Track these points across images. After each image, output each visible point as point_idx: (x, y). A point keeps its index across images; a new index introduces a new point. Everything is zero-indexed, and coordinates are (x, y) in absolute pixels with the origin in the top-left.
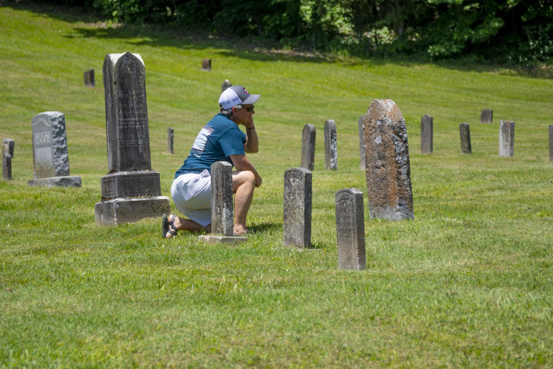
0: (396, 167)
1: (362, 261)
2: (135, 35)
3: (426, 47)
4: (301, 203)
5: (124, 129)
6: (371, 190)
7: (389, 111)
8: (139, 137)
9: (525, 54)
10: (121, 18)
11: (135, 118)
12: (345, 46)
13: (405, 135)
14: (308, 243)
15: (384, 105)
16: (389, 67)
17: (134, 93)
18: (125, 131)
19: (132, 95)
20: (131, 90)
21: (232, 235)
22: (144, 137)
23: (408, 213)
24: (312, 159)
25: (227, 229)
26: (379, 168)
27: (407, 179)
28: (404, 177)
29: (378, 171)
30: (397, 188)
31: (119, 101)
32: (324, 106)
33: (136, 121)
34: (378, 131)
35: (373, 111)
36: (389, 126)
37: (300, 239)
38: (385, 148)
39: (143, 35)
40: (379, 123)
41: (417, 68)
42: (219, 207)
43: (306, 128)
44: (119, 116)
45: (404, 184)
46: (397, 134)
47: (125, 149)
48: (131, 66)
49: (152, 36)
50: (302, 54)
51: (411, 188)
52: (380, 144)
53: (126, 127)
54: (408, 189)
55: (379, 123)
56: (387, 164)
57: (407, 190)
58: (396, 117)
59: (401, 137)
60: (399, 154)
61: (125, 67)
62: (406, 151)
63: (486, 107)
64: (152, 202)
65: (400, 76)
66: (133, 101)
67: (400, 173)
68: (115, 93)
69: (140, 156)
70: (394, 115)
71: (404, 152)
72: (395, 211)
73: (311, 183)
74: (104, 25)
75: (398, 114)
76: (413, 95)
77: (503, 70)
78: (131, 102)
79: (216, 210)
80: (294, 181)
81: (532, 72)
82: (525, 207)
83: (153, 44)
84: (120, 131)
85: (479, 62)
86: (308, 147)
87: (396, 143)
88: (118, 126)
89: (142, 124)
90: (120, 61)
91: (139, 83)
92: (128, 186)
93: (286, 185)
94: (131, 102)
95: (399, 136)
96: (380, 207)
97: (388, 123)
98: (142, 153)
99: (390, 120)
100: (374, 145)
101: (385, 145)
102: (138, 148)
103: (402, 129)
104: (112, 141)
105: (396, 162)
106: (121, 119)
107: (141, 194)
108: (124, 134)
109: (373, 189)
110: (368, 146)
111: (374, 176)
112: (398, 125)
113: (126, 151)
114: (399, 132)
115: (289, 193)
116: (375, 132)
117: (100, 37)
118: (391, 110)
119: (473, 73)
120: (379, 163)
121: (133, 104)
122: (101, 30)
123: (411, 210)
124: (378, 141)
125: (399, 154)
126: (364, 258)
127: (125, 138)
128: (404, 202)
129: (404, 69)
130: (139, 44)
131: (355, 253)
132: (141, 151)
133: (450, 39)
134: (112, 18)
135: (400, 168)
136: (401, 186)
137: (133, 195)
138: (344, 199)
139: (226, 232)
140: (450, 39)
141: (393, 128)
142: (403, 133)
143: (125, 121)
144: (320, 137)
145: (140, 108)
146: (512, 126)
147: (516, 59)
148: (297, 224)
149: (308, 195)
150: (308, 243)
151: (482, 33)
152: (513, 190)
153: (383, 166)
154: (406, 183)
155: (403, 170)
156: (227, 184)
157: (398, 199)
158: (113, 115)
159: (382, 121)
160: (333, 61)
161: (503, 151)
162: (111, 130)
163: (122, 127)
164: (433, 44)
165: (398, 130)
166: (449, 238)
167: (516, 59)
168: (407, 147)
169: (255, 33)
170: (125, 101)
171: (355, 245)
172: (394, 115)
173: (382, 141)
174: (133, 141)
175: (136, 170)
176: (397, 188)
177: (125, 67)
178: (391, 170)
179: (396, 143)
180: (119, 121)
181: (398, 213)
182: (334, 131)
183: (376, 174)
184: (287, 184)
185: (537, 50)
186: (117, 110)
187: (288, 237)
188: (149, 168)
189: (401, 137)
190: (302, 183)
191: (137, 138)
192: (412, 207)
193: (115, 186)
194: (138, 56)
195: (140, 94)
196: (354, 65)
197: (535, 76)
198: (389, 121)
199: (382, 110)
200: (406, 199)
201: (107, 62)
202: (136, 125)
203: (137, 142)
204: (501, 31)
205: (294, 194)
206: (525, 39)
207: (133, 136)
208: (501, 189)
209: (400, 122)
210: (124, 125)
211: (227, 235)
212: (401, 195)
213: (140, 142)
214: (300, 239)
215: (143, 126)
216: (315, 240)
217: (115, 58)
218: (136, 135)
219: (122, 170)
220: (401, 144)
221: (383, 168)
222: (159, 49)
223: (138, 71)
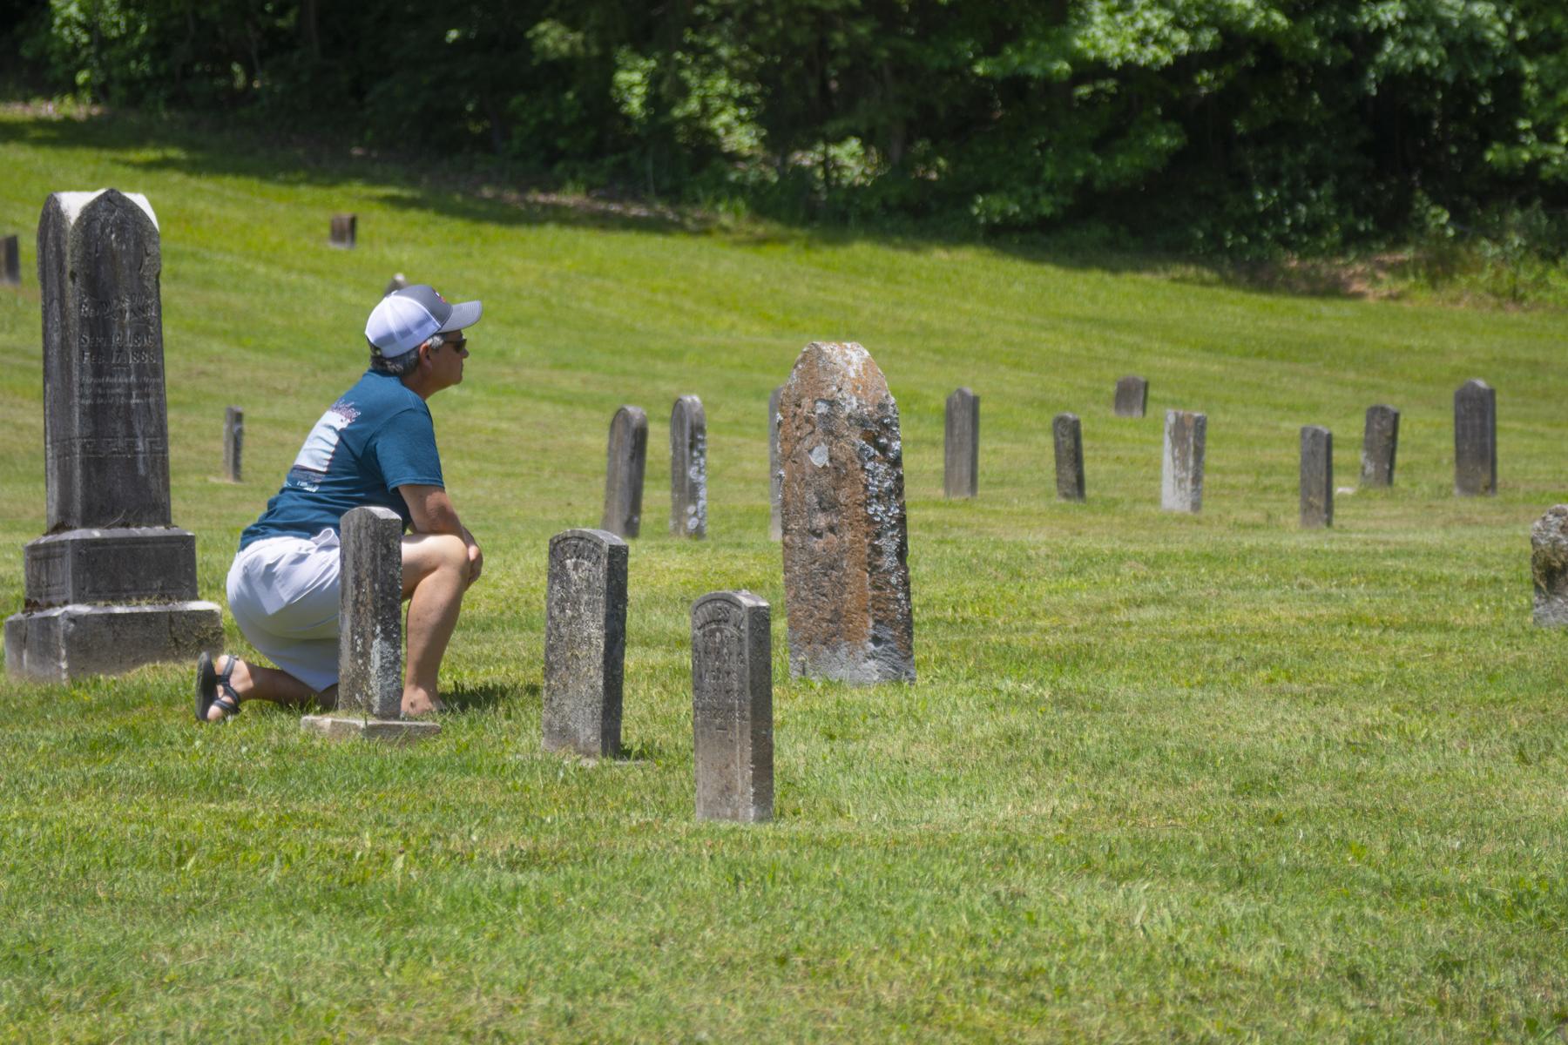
1: (763, 797)
2: (139, 141)
3: (965, 199)
4: (594, 630)
5: (94, 407)
6: (796, 596)
7: (853, 375)
8: (138, 432)
9: (1241, 226)
10: (101, 92)
11: (129, 376)
12: (738, 189)
13: (896, 445)
14: (613, 745)
15: (839, 360)
16: (862, 251)
17: (126, 305)
18: (98, 413)
19: (122, 312)
20: (118, 298)
21: (397, 717)
23: (900, 663)
24: (635, 505)
25: (382, 700)
26: (820, 536)
28: (888, 562)
29: (818, 545)
31: (82, 326)
32: (674, 355)
33: (129, 387)
34: (819, 430)
35: (807, 375)
36: (850, 417)
37: (588, 732)
38: (839, 479)
39: (162, 141)
41: (939, 257)
42: (362, 635)
43: (621, 416)
44: (82, 370)
45: (888, 583)
46: (873, 440)
47: (96, 464)
48: (121, 228)
49: (189, 145)
50: (615, 208)
51: (908, 593)
52: (824, 467)
53: (100, 401)
54: (900, 595)
55: (822, 408)
57: (898, 600)
58: (871, 394)
59: (884, 449)
60: (878, 497)
62: (898, 490)
63: (1129, 372)
64: (172, 617)
65: (891, 277)
66: (122, 327)
67: (878, 551)
70: (865, 387)
71: (891, 491)
72: (861, 658)
74: (49, 109)
76: (926, 332)
77: (1179, 270)
80: (576, 567)
81: (1256, 274)
82: (1225, 654)
83: (193, 168)
84: (83, 413)
85: (1113, 245)
86: (623, 471)
89: (148, 395)
90: (90, 212)
91: (141, 278)
92: (103, 571)
94: (116, 329)
95: (877, 446)
96: (819, 647)
97: (848, 410)
98: (146, 479)
100: (808, 471)
101: (837, 470)
103: (887, 427)
104: (60, 442)
106: (88, 380)
107: (141, 593)
108: (96, 423)
109: (803, 594)
111: (805, 557)
112: (876, 416)
114: (880, 436)
115: (562, 600)
117: (38, 143)
118: (857, 372)
119: (1095, 276)
120: (821, 521)
121: (123, 337)
122: (41, 123)
123: (908, 657)
124: (819, 458)
125: (878, 497)
128: (887, 633)
129: (906, 259)
130: (149, 166)
131: (743, 774)
132: (142, 471)
133: (1034, 178)
134: (74, 89)
135: (878, 536)
136: (880, 588)
137: (116, 599)
138: (718, 620)
139: (381, 707)
140: (1034, 178)
141: (862, 422)
144: (659, 443)
146: (1200, 426)
147: (1215, 238)
148: (583, 688)
150: (613, 745)
151: (1124, 164)
152: (1196, 607)
153: (831, 529)
154: (893, 580)
155: (889, 544)
157: (871, 623)
158: (66, 367)
159: (832, 403)
160: (704, 229)
161: (1173, 496)
162: (57, 408)
163: (88, 402)
164: (985, 189)
165: (875, 428)
166: (1011, 738)
167: (1215, 238)
168: (900, 479)
169: (484, 143)
170: (99, 327)
171: (743, 755)
172: (865, 387)
173: (831, 459)
175: (127, 525)
178: (852, 542)
179: (869, 466)
180: (82, 385)
181: (872, 663)
182: (698, 429)
183: (812, 552)
184: (557, 574)
185: (1274, 214)
186: (75, 353)
188: (166, 521)
189: (884, 449)
190: (601, 572)
191: (131, 434)
192: (910, 648)
193: (65, 571)
194: (140, 200)
195: (143, 309)
196: (761, 241)
197: (1267, 287)
198: (851, 404)
199: (832, 372)
200: (893, 623)
201: (51, 215)
202: (129, 396)
203: (132, 446)
204: (1176, 158)
205: (576, 603)
206: (1242, 183)
207: (120, 427)
208: (1161, 601)
210: (95, 396)
211: (382, 716)
213: (141, 446)
214: (589, 731)
215: (152, 400)
216: (631, 735)
217: (74, 203)
218: (129, 425)
219: (87, 523)
220: (882, 468)
221: (831, 535)
222: (207, 184)
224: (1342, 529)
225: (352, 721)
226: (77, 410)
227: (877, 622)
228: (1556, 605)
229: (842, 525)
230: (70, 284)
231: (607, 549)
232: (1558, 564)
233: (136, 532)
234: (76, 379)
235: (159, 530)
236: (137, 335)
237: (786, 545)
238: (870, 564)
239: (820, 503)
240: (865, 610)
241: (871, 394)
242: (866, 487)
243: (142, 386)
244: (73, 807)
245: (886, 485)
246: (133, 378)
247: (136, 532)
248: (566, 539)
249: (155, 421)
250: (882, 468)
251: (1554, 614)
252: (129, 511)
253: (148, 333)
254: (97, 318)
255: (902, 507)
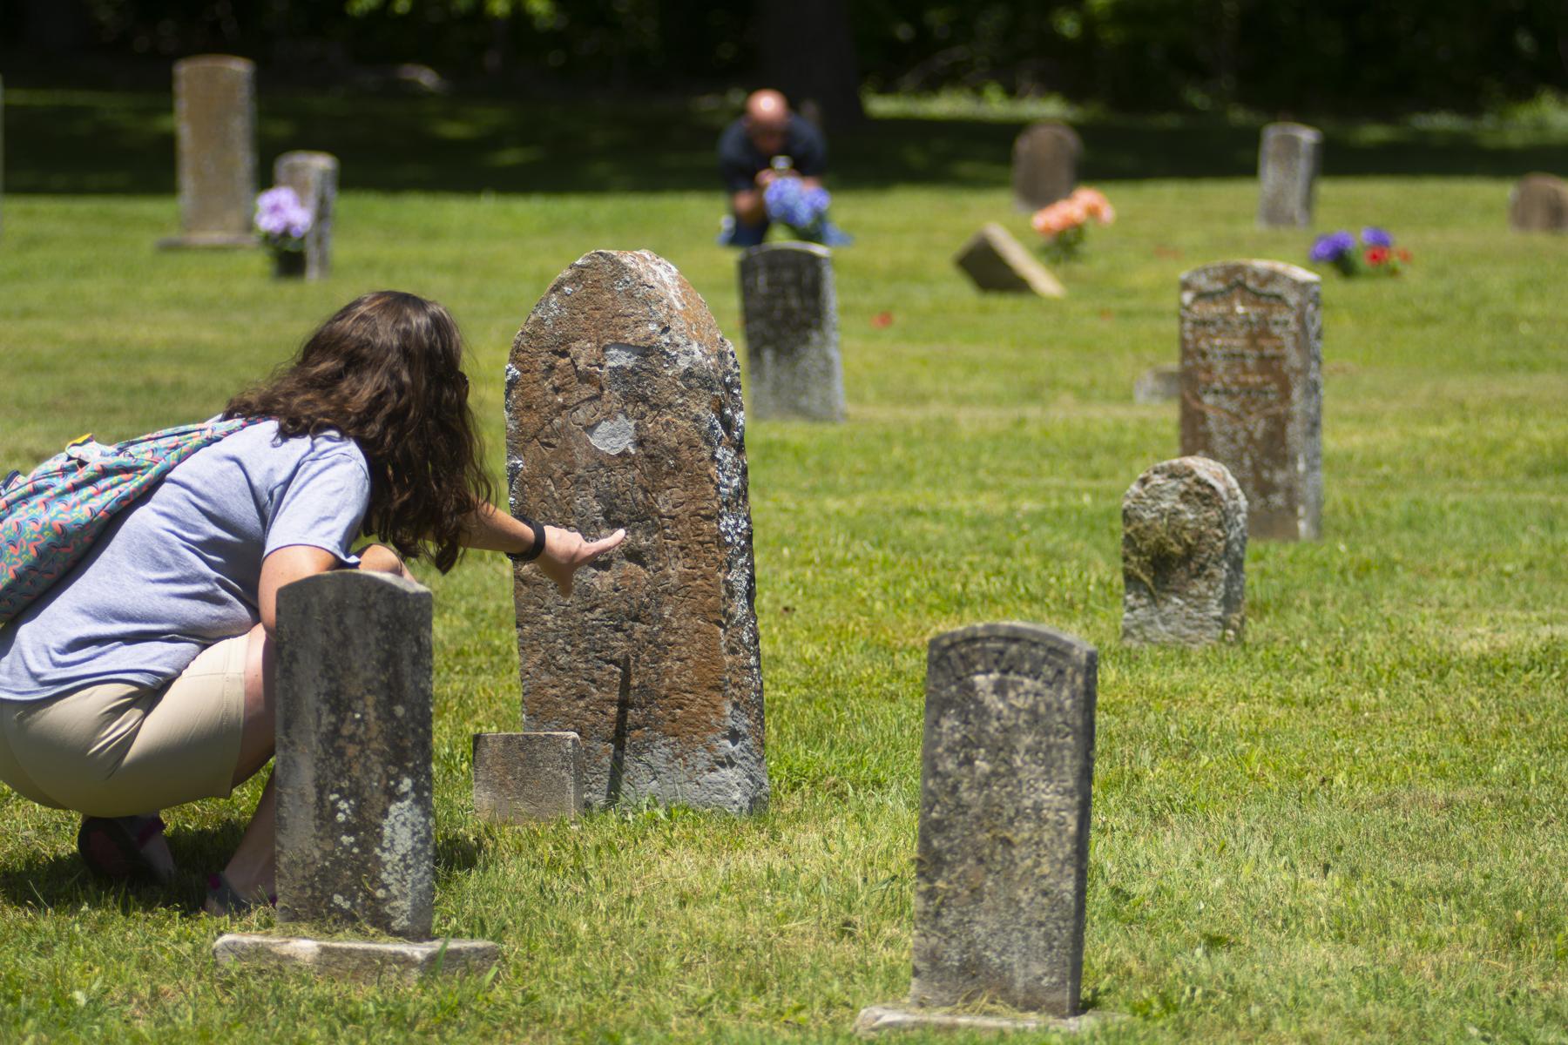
6: (546, 665)
36: (688, 374)
37: (1033, 968)
38: (656, 474)
42: (354, 793)
52: (624, 454)
55: (621, 359)
79: (325, 814)
80: (1000, 689)
93: (937, 706)
97: (683, 363)
100: (582, 459)
109: (562, 659)
115: (966, 743)
156: (416, 684)
173: (640, 443)
178: (685, 577)
187: (953, 957)
199: (646, 302)
205: (1002, 749)
214: (1038, 969)
216: (1096, 978)
221: (631, 567)
224: (1090, 524)
225: (277, 942)
228: (1169, 609)
232: (1177, 549)
239: (606, 514)
248: (972, 640)
251: (1165, 622)
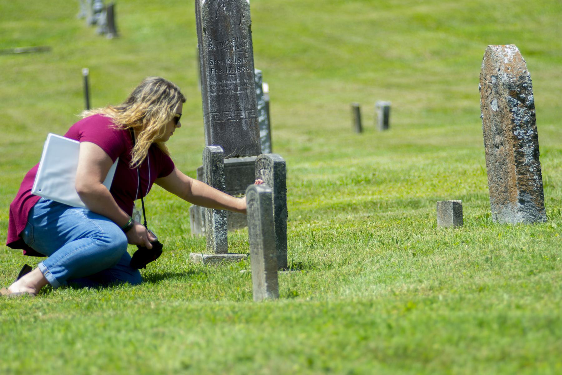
0: (514, 146)
5: (218, 96)
6: (491, 180)
7: (506, 61)
8: (242, 108)
11: (236, 80)
13: (530, 98)
15: (500, 54)
17: (233, 43)
19: (231, 47)
20: (228, 40)
21: (226, 252)
22: (249, 107)
23: (536, 213)
25: (217, 244)
27: (533, 163)
28: (527, 160)
29: (497, 152)
30: (517, 177)
31: (210, 56)
33: (236, 85)
34: (493, 92)
40: (494, 80)
44: (211, 78)
45: (528, 170)
46: (516, 95)
51: (540, 176)
53: (220, 94)
54: (535, 177)
55: (494, 80)
56: (505, 141)
57: (534, 180)
58: (516, 71)
59: (523, 100)
60: (520, 126)
61: (219, 6)
62: (533, 121)
66: (231, 55)
67: (521, 155)
68: (204, 45)
69: (244, 135)
70: (513, 68)
71: (528, 122)
72: (516, 211)
73: (284, 177)
75: (519, 66)
78: (228, 57)
80: (264, 172)
84: (212, 100)
87: (514, 109)
88: (209, 93)
89: (246, 89)
91: (240, 29)
94: (228, 56)
95: (519, 99)
96: (501, 206)
97: (503, 81)
98: (247, 131)
99: (505, 75)
100: (491, 113)
102: (240, 124)
103: (525, 88)
105: (515, 138)
106: (215, 83)
108: (219, 104)
110: (486, 115)
111: (493, 159)
112: (518, 83)
113: (221, 129)
114: (520, 93)
116: (491, 93)
118: (509, 60)
120: (498, 139)
121: (232, 58)
123: (541, 207)
125: (520, 126)
126: (277, 284)
127: (219, 111)
128: (528, 198)
132: (245, 128)
135: (521, 146)
136: (523, 174)
139: (217, 247)
142: (527, 95)
143: (220, 85)
145: (243, 65)
149: (279, 193)
154: (531, 169)
155: (528, 150)
157: (518, 192)
159: (497, 77)
163: (215, 94)
165: (517, 90)
168: (533, 115)
172: (513, 68)
173: (498, 107)
174: (233, 114)
175: (238, 156)
176: (517, 177)
177: (219, 6)
179: (514, 109)
180: (211, 86)
181: (520, 213)
186: (207, 69)
189: (523, 100)
191: (238, 110)
192: (542, 205)
195: (242, 45)
198: (505, 78)
200: (531, 192)
202: (237, 90)
203: (239, 115)
207: (232, 106)
209: (522, 77)
210: (218, 91)
211: (218, 252)
212: (524, 187)
213: (243, 115)
215: (248, 91)
218: (237, 105)
220: (522, 111)
223: (239, 10)
226: (209, 98)
227: (521, 192)
229: (505, 141)
230: (203, 34)
231: (273, 164)
233: (241, 159)
234: (208, 83)
235: (254, 158)
236: (239, 58)
237: (486, 153)
238: (516, 161)
240: (516, 186)
241: (516, 71)
242: (513, 121)
243: (243, 84)
244: (431, 282)
245: (525, 119)
246: (238, 81)
247: (241, 159)
249: (251, 102)
250: (522, 111)
252: (238, 149)
253: (245, 57)
254: (218, 51)
255: (535, 130)
